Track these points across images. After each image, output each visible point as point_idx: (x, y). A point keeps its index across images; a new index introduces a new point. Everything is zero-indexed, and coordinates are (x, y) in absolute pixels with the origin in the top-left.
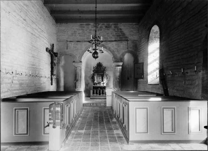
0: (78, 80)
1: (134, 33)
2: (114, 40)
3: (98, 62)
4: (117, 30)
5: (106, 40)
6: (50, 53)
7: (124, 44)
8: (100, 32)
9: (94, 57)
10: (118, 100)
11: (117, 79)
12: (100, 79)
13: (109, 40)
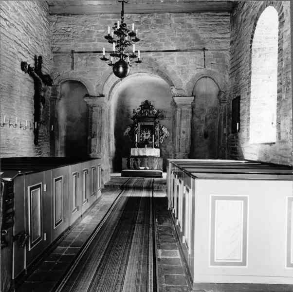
0: (96, 135)
1: (221, 34)
2: (174, 49)
3: (144, 101)
4: (182, 27)
5: (158, 50)
6: (32, 75)
7: (196, 57)
8: (144, 33)
9: (117, 74)
10: (180, 182)
11: (182, 132)
12: (147, 135)
13: (164, 48)
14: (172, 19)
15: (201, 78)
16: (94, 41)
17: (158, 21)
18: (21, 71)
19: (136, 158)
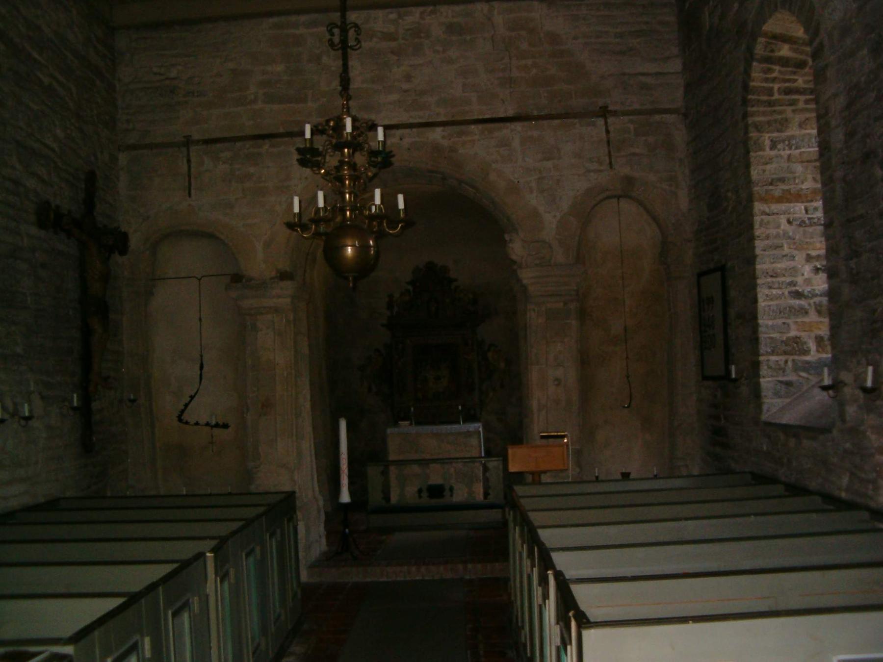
2: (511, 113)
14: (498, 19)
15: (601, 201)
16: (254, 101)
17: (451, 28)
18: (34, 230)
19: (822, 371)
